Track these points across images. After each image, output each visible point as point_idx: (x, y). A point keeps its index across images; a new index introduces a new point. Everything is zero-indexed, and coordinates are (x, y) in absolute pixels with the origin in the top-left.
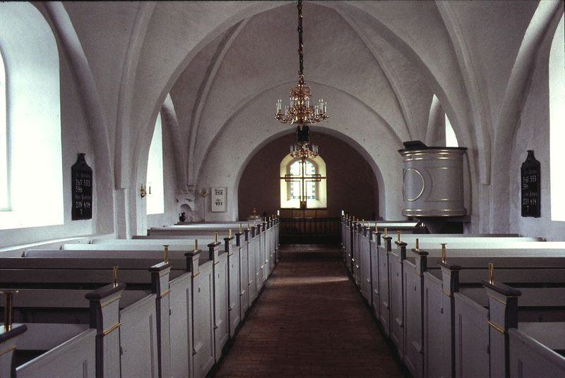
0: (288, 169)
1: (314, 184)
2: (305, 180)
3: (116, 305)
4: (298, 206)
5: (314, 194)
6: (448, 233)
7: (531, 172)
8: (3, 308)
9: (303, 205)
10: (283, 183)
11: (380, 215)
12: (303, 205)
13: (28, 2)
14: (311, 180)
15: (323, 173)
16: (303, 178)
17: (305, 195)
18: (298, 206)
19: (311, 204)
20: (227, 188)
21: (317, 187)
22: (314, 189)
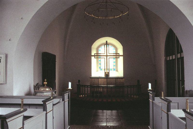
0: (97, 49)
1: (115, 60)
2: (108, 57)
3: (51, 105)
4: (103, 75)
5: (115, 67)
6: (101, 38)
7: (121, 87)
8: (21, 104)
9: (107, 75)
10: (93, 60)
11: (29, 90)
12: (107, 75)
13: (122, 47)
14: (101, 55)
15: (121, 52)
16: (107, 56)
17: (108, 68)
18: (103, 75)
19: (113, 74)
20: (6, 56)
21: (116, 62)
22: (115, 64)
